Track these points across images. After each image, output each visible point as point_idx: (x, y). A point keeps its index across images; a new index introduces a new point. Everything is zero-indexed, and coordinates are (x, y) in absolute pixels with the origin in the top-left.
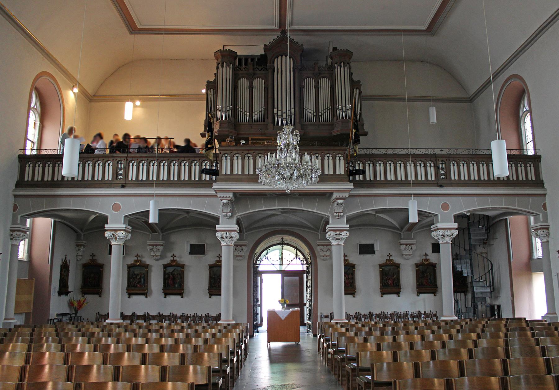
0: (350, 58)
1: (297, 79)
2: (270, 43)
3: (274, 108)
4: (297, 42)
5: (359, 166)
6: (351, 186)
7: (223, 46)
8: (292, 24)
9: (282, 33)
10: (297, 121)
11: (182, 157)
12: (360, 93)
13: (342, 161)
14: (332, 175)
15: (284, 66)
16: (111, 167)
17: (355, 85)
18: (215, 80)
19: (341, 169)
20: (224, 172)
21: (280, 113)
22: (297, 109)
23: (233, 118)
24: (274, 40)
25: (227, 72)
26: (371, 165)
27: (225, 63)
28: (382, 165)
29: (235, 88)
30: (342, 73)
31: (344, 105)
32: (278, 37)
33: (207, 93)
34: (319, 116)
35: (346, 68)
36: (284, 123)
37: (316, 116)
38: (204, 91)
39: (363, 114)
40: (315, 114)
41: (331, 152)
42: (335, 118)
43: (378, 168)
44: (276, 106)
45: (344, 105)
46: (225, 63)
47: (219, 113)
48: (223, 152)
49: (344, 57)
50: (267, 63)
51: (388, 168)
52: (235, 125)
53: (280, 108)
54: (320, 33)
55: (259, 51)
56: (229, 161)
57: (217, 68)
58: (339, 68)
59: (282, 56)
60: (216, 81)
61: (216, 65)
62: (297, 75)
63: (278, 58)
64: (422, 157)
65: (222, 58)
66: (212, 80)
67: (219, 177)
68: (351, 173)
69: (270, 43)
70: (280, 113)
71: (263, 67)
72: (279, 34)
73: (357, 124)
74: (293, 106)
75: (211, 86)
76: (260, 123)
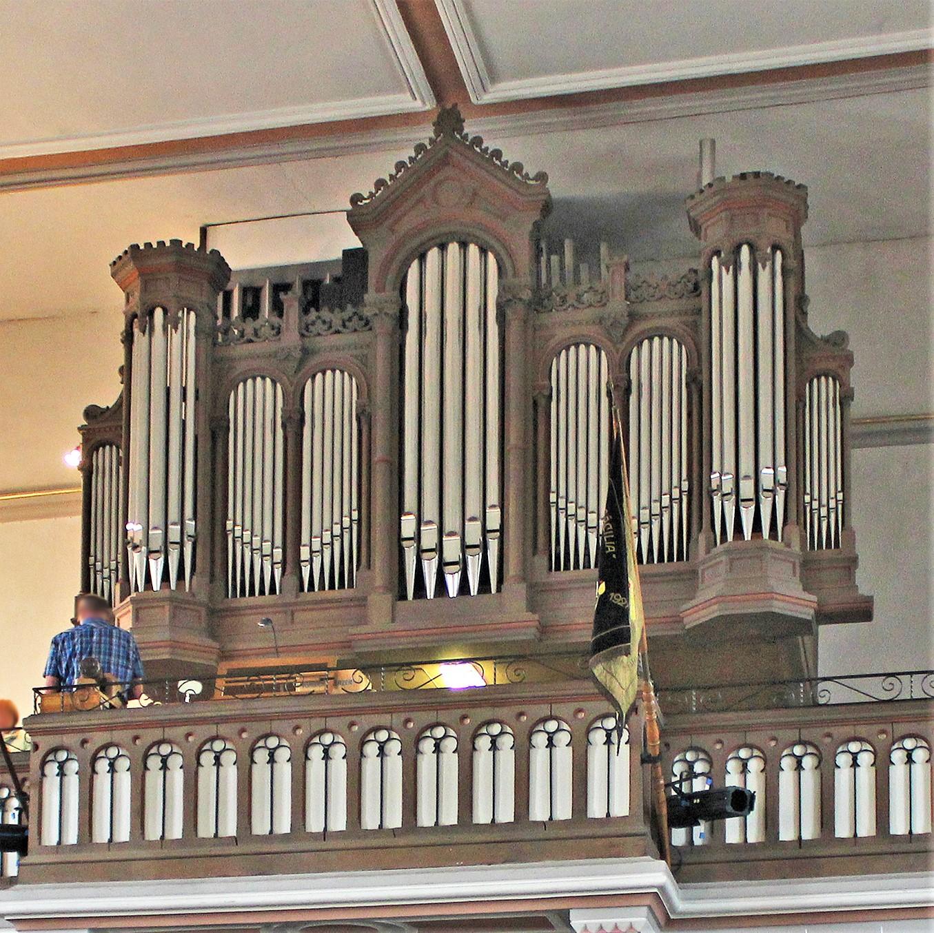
0: (797, 217)
1: (705, 339)
2: (380, 183)
3: (226, 517)
4: (518, 167)
5: (744, 770)
6: (655, 874)
7: (204, 232)
8: (399, 83)
9: (439, 126)
10: (512, 569)
11: (735, 729)
12: (845, 399)
13: (623, 758)
14: (394, 832)
15: (454, 289)
16: (921, 771)
17: (812, 358)
18: (119, 405)
19: (614, 790)
20: (51, 838)
21: (429, 540)
22: (512, 508)
23: (201, 580)
24: (400, 165)
25: (175, 350)
26: (808, 762)
27: (159, 313)
28: (866, 759)
29: (215, 431)
30: (742, 301)
31: (747, 467)
32: (420, 148)
33: (88, 470)
34: (298, 562)
35: (764, 276)
36: (453, 583)
37: (284, 562)
38: (74, 458)
39: (854, 509)
40: (278, 554)
41: (564, 710)
42: (702, 539)
43: (843, 777)
44: (553, 487)
45: (747, 467)
46: (745, 250)
47: (137, 560)
48: (46, 742)
49: (768, 212)
50: (364, 288)
51: (898, 773)
52: (212, 612)
53: (430, 512)
54: (649, 106)
55: (334, 240)
56: (73, 782)
57: (128, 339)
58: (728, 279)
59: (443, 247)
60: (125, 401)
61: (121, 326)
62: (514, 328)
63: (422, 258)
64: (857, 722)
65: (145, 289)
66: (107, 400)
67: (29, 859)
68: (677, 816)
69: (380, 183)
70: (429, 540)
71: (350, 310)
72: (426, 133)
73: (827, 554)
74: (493, 497)
75: (104, 429)
76: (328, 594)
